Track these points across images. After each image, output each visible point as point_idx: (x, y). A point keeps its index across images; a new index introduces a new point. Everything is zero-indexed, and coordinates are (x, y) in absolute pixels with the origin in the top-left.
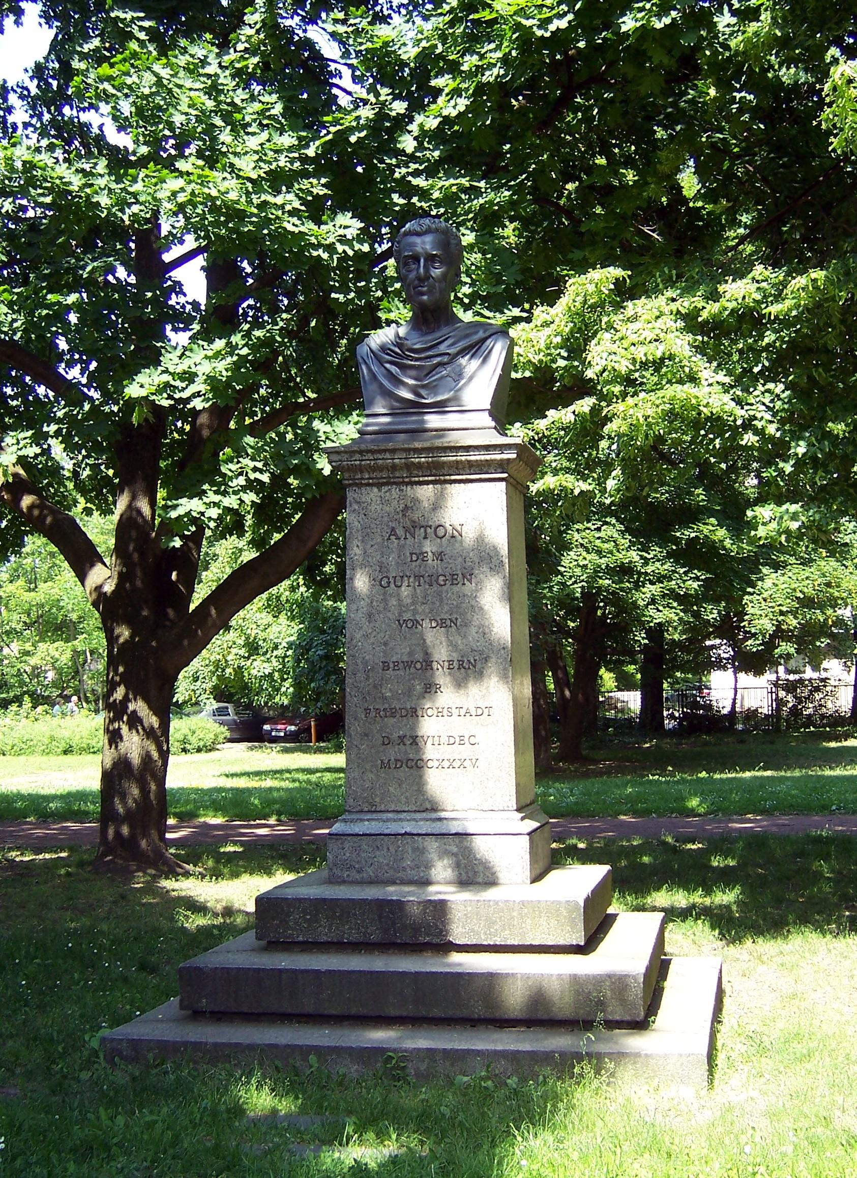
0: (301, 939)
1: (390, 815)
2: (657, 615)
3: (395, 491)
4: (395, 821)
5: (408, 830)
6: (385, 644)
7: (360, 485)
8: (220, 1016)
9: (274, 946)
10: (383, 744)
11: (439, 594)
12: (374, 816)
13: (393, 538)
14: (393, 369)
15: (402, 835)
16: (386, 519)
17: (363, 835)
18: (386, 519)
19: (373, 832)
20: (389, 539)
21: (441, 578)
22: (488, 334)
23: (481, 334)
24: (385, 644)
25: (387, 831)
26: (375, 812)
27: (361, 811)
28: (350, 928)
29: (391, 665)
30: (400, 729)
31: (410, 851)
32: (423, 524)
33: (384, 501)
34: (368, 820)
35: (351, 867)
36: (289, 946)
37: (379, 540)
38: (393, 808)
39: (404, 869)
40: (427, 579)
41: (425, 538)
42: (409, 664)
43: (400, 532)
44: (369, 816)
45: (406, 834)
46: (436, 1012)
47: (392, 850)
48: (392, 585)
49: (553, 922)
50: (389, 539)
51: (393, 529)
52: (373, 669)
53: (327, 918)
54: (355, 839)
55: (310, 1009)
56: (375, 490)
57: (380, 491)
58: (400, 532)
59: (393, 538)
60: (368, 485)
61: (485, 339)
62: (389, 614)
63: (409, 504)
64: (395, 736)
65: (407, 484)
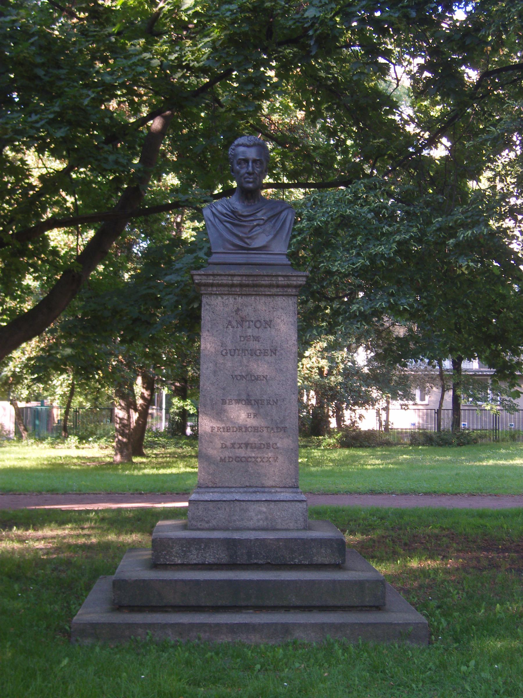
0: (179, 562)
1: (225, 490)
2: (75, 404)
3: (231, 300)
4: (228, 493)
5: (237, 498)
6: (224, 389)
7: (211, 294)
8: (133, 609)
9: (155, 565)
10: (222, 448)
12: (216, 490)
13: (230, 327)
14: (228, 225)
15: (233, 501)
16: (225, 315)
17: (211, 501)
18: (225, 315)
19: (216, 499)
20: (227, 327)
21: (258, 351)
22: (283, 208)
23: (279, 209)
24: (224, 389)
25: (224, 499)
26: (216, 487)
27: (208, 487)
28: (210, 555)
31: (238, 510)
32: (248, 319)
33: (225, 305)
34: (212, 492)
35: (202, 520)
36: (165, 567)
37: (221, 328)
39: (235, 521)
40: (249, 352)
41: (249, 327)
43: (234, 323)
44: (212, 490)
45: (236, 500)
46: (268, 603)
47: (227, 510)
48: (229, 355)
49: (329, 551)
50: (227, 327)
51: (230, 322)
52: (216, 403)
53: (196, 549)
54: (205, 503)
55: (193, 602)
56: (220, 298)
57: (222, 298)
58: (234, 323)
59: (230, 327)
60: (216, 294)
61: (281, 212)
62: (226, 372)
63: (240, 308)
65: (239, 295)
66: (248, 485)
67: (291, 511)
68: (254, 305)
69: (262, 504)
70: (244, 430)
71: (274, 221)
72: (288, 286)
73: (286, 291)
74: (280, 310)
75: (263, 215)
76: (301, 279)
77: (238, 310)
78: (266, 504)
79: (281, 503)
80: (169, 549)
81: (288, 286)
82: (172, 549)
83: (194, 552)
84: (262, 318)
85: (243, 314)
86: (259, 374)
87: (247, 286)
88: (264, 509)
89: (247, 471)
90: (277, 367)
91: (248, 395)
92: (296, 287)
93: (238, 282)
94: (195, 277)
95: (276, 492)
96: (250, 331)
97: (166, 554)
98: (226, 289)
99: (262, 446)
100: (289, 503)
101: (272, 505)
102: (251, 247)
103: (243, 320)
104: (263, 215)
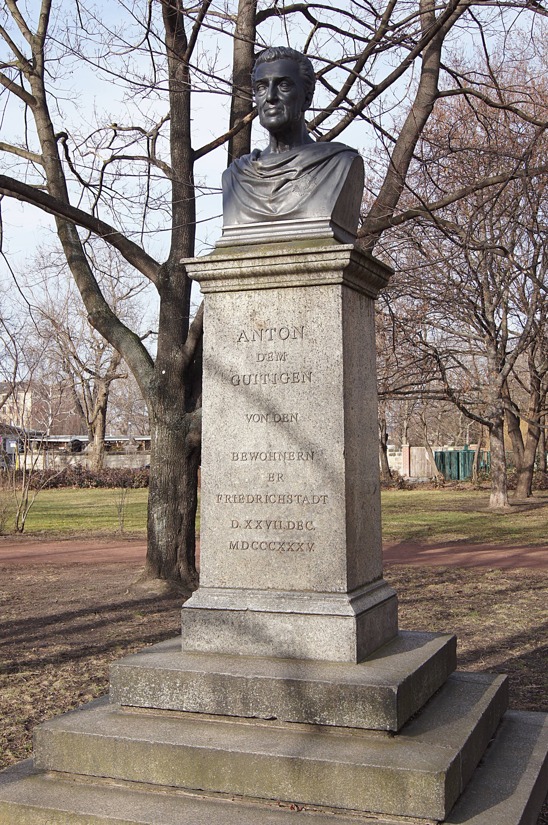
6: (235, 437)
11: (282, 391)
29: (240, 456)
30: (246, 514)
38: (240, 585)
41: (271, 339)
42: (255, 456)
63: (257, 310)
64: (242, 522)
66: (270, 586)
67: (329, 631)
68: (277, 304)
69: (286, 618)
70: (263, 499)
71: (312, 174)
72: (325, 269)
73: (325, 278)
74: (317, 309)
75: (297, 165)
76: (341, 255)
77: (254, 312)
78: (292, 619)
79: (315, 617)
80: (132, 684)
81: (325, 269)
82: (137, 684)
83: (166, 690)
84: (289, 323)
85: (261, 318)
86: (285, 411)
87: (264, 274)
88: (290, 627)
89: (269, 564)
90: (311, 399)
91: (270, 446)
92: (336, 269)
93: (249, 269)
94: (189, 268)
95: (102, 623)
96: (271, 344)
97: (129, 692)
98: (236, 282)
99: (291, 526)
100: (326, 618)
101: (301, 621)
102: (276, 215)
103: (262, 329)
104: (297, 165)
